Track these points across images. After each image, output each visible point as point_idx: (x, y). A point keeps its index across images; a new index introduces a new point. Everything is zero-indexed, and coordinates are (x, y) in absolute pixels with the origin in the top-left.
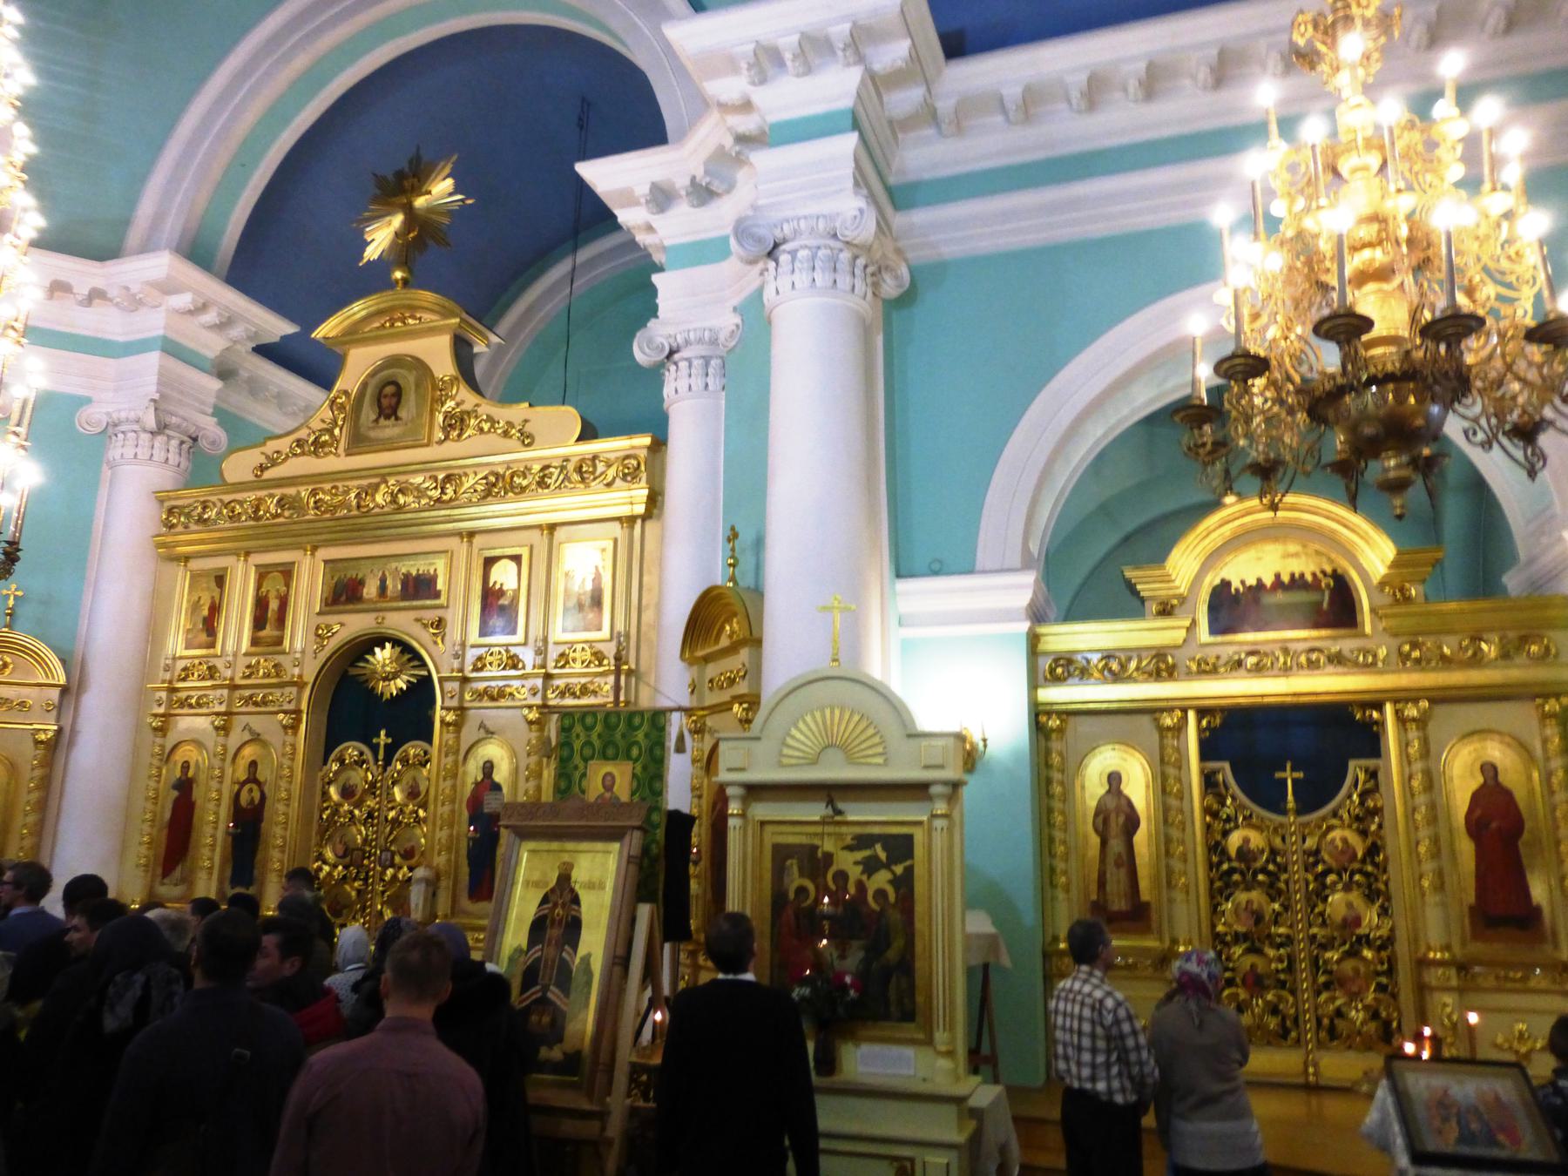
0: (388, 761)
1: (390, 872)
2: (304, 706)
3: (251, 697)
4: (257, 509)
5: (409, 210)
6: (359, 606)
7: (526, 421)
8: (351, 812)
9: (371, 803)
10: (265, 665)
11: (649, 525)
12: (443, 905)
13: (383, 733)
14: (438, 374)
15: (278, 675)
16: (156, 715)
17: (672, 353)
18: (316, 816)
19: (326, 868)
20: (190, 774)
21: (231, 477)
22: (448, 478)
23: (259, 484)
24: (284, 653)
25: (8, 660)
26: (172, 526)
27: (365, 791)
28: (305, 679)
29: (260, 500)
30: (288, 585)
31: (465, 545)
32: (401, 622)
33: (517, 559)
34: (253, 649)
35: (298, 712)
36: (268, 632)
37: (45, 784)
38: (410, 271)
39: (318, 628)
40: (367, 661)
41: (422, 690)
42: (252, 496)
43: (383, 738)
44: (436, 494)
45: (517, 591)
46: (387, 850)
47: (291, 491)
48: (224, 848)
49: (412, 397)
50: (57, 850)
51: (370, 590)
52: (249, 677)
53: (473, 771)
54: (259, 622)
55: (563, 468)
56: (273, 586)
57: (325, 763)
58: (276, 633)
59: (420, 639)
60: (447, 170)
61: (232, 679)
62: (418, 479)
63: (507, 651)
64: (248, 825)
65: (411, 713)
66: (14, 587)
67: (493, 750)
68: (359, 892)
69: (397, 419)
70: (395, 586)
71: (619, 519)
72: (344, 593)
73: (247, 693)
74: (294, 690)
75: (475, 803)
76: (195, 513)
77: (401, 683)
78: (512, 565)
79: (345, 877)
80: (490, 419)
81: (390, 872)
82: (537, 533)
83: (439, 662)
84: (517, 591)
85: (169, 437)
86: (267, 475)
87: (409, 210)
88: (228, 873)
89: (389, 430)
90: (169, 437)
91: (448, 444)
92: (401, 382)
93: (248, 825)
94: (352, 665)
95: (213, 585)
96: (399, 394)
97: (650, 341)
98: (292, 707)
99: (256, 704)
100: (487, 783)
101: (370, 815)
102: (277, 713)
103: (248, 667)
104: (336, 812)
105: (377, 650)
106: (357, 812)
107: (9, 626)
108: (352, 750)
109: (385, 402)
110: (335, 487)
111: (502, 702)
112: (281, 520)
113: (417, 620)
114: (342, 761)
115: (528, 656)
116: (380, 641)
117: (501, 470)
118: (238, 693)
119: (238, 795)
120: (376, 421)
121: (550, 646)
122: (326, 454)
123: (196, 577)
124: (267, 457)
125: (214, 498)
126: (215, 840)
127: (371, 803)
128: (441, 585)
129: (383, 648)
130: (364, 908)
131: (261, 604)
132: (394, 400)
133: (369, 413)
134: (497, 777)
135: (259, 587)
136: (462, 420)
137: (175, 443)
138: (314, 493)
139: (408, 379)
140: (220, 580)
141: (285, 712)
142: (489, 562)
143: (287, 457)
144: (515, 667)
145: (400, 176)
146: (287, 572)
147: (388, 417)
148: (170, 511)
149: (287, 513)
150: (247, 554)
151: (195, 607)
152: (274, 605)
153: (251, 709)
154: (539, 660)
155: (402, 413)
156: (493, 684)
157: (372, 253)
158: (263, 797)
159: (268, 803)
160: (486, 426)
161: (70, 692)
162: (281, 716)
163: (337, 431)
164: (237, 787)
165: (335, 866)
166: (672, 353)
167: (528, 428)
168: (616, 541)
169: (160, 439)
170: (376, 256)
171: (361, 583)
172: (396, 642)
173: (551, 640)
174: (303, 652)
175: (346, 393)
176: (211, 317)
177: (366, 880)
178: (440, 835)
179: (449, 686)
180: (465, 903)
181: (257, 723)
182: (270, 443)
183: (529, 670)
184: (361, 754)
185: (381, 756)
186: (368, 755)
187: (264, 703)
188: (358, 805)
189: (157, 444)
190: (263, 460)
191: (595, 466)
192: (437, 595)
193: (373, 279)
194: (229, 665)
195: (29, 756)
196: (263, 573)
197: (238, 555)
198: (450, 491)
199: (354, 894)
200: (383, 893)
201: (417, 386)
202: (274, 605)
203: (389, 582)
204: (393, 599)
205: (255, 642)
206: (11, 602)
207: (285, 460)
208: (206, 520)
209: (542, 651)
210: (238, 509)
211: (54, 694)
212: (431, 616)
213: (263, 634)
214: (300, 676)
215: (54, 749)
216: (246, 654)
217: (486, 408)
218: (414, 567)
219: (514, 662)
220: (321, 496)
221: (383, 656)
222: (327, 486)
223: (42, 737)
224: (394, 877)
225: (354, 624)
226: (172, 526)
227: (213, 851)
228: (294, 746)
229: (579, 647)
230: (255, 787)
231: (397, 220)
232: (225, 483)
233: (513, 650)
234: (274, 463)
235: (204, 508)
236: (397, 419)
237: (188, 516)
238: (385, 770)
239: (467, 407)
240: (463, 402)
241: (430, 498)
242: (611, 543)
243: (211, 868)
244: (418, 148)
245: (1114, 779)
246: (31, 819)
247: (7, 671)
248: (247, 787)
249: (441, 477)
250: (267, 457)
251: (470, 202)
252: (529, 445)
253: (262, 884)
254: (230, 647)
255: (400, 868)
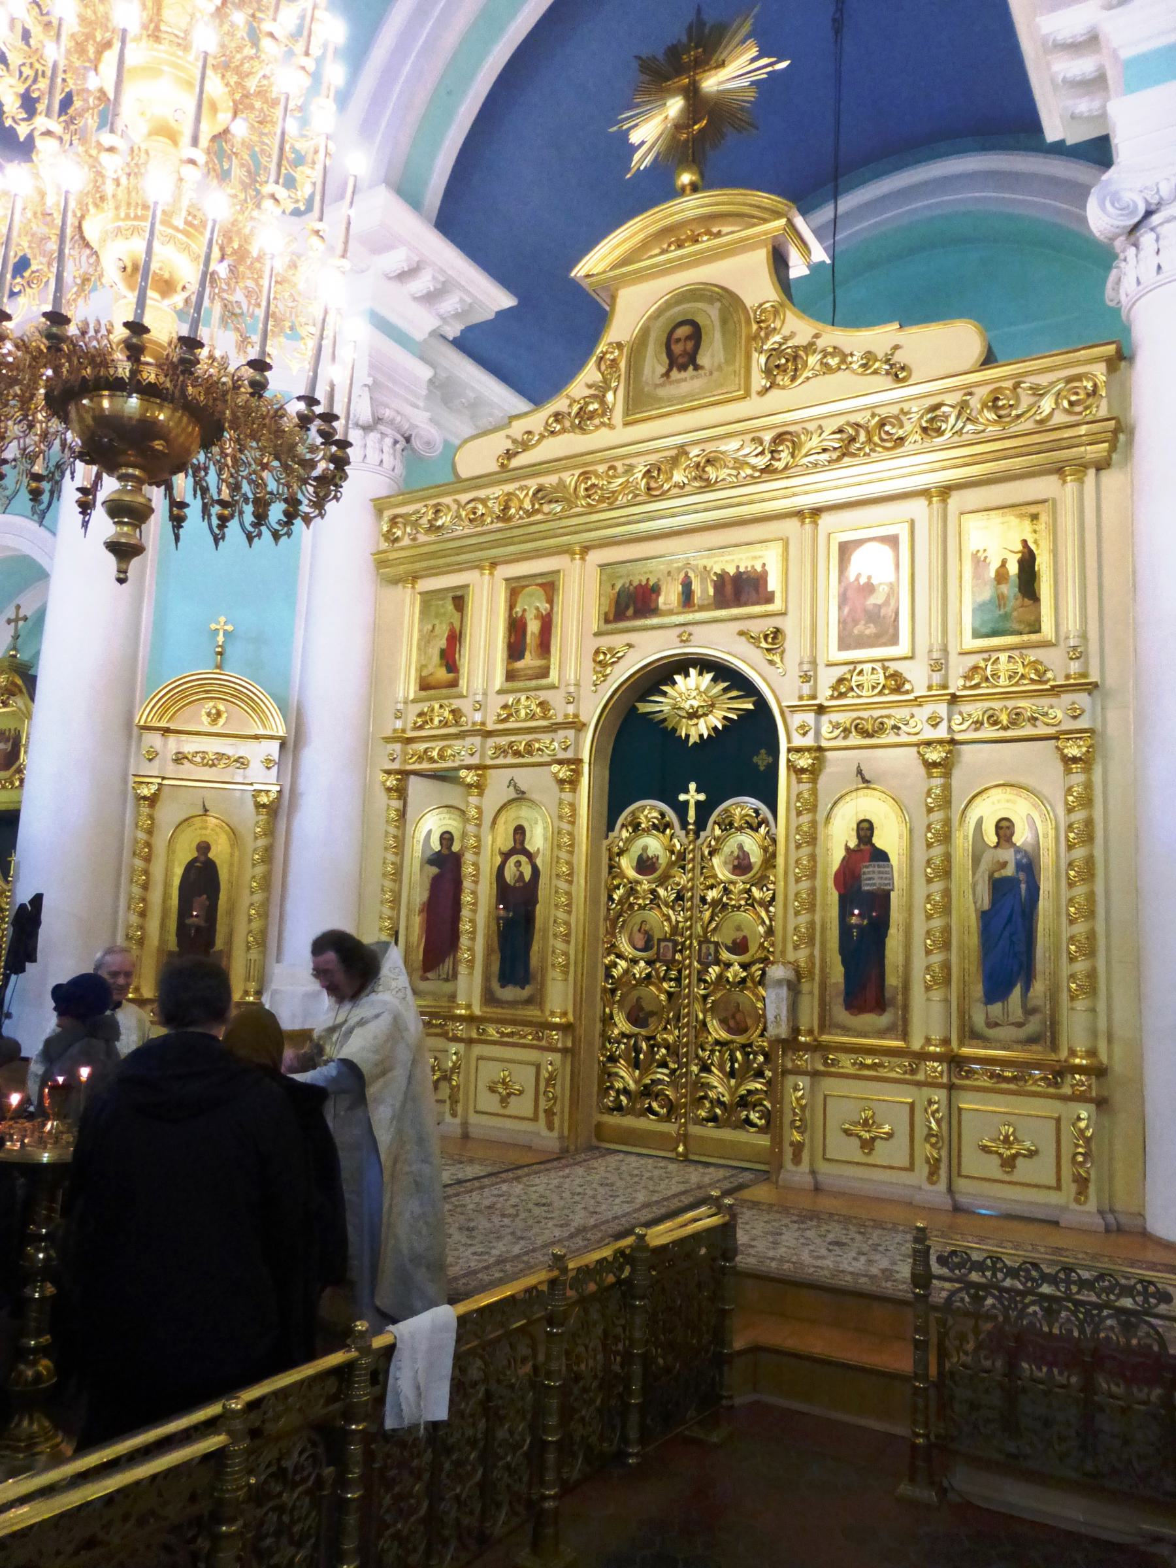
0: (701, 824)
1: (714, 971)
2: (585, 756)
3: (511, 745)
4: (506, 508)
5: (692, 93)
6: (655, 621)
7: (896, 347)
8: (653, 892)
9: (682, 879)
10: (526, 704)
11: (1110, 479)
12: (809, 1016)
13: (692, 786)
14: (750, 301)
15: (544, 718)
16: (388, 772)
17: (1149, 213)
18: (604, 898)
19: (623, 964)
20: (456, 848)
21: (466, 470)
22: (779, 439)
23: (505, 471)
24: (461, 696)
25: (221, 707)
26: (397, 540)
27: (671, 864)
28: (583, 719)
29: (509, 496)
30: (550, 601)
31: (486, 577)
32: (720, 638)
33: (892, 541)
34: (509, 685)
35: (578, 761)
36: (529, 661)
37: (268, 856)
38: (702, 175)
39: (597, 652)
40: (664, 694)
41: (754, 730)
42: (498, 491)
43: (692, 796)
44: (761, 462)
45: (893, 590)
46: (708, 941)
47: (550, 480)
48: (488, 937)
49: (718, 335)
50: (287, 935)
51: (669, 596)
52: (421, 728)
53: (839, 837)
54: (515, 650)
55: (963, 406)
56: (532, 606)
57: (611, 827)
58: (539, 663)
59: (747, 660)
60: (746, 28)
61: (483, 724)
62: (731, 445)
63: (885, 669)
64: (518, 905)
65: (743, 756)
66: (222, 619)
67: (869, 805)
68: (670, 995)
69: (697, 368)
70: (704, 591)
71: (925, 493)
72: (633, 603)
73: (422, 747)
74: (571, 733)
75: (848, 878)
76: (424, 521)
77: (715, 720)
78: (886, 550)
79: (649, 975)
80: (837, 351)
81: (714, 971)
82: (922, 502)
83: (779, 686)
84: (893, 590)
85: (383, 435)
86: (515, 462)
87: (692, 93)
88: (496, 968)
89: (686, 383)
90: (383, 435)
91: (774, 392)
92: (700, 320)
93: (518, 905)
94: (643, 699)
95: (450, 607)
96: (697, 334)
97: (1115, 198)
98: (569, 755)
99: (517, 754)
100: (866, 848)
101: (680, 897)
102: (548, 764)
103: (505, 707)
104: (632, 891)
105: (678, 678)
106: (661, 892)
107: (219, 667)
108: (649, 810)
109: (677, 349)
110: (612, 468)
111: (883, 739)
112: (539, 517)
113: (742, 633)
114: (636, 826)
115: (918, 676)
116: (682, 665)
117: (858, 418)
118: (491, 742)
119: (501, 869)
120: (667, 374)
121: (821, 669)
122: (597, 427)
123: (428, 598)
124: (515, 441)
125: (447, 500)
126: (474, 926)
127: (682, 879)
128: (774, 584)
129: (687, 675)
130: (678, 1018)
131: (516, 627)
132: (690, 345)
133: (654, 364)
134: (879, 841)
135: (511, 607)
136: (796, 357)
137: (388, 441)
138: (585, 475)
139: (709, 315)
140: (459, 601)
141: (561, 762)
142: (845, 550)
143: (542, 437)
144: (898, 690)
145: (674, 52)
146: (549, 586)
147: (683, 368)
148: (393, 521)
149: (546, 508)
150: (493, 565)
151: (426, 639)
152: (533, 627)
153: (510, 760)
154: (937, 678)
155: (704, 359)
156: (865, 714)
157: (641, 160)
158: (536, 872)
159: (543, 881)
160: (833, 362)
161: (291, 747)
162: (555, 768)
163: (610, 396)
164: (498, 860)
165: (634, 961)
166: (1149, 213)
167: (899, 357)
168: (912, 523)
169: (373, 436)
170: (647, 162)
171: (655, 590)
172: (705, 665)
173: (953, 650)
174: (577, 685)
175: (619, 345)
176: (423, 283)
177: (678, 980)
178: (801, 923)
179: (797, 719)
180: (840, 1014)
181: (524, 778)
182: (515, 424)
183: (921, 691)
184: (663, 815)
185: (692, 815)
186: (671, 816)
187: (529, 751)
188: (663, 881)
189: (370, 443)
190: (509, 445)
191: (1018, 398)
192: (769, 599)
193: (657, 187)
194: (479, 706)
195: (250, 820)
196: (515, 589)
197: (481, 568)
198: (785, 456)
199: (663, 997)
200: (705, 997)
201: (724, 321)
202: (533, 627)
203: (696, 586)
204: (702, 608)
205: (510, 676)
206: (221, 639)
207: (539, 441)
208: (439, 527)
209: (939, 666)
210: (481, 509)
211: (273, 748)
212: (758, 627)
213: (520, 664)
214: (576, 716)
215: (275, 812)
216: (500, 692)
217: (833, 337)
218: (731, 563)
219: (897, 683)
220: (594, 480)
221: (690, 688)
222: (601, 469)
223: (263, 799)
224: (720, 976)
225: (648, 645)
226: (397, 540)
227: (473, 939)
228: (573, 807)
229: (867, 667)
230: (523, 859)
231: (675, 106)
232: (459, 479)
233: (893, 666)
234: (525, 446)
235: (437, 511)
236: (697, 368)
237: (415, 524)
238: (697, 836)
239: (801, 340)
240: (793, 335)
241: (754, 468)
242: (906, 526)
243: (567, 966)
244: (699, 11)
245: (865, 830)
246: (258, 897)
247: (222, 721)
248: (513, 860)
249: (767, 437)
250: (515, 441)
251: (784, 65)
252: (904, 380)
253: (543, 984)
254: (478, 684)
255: (728, 965)
